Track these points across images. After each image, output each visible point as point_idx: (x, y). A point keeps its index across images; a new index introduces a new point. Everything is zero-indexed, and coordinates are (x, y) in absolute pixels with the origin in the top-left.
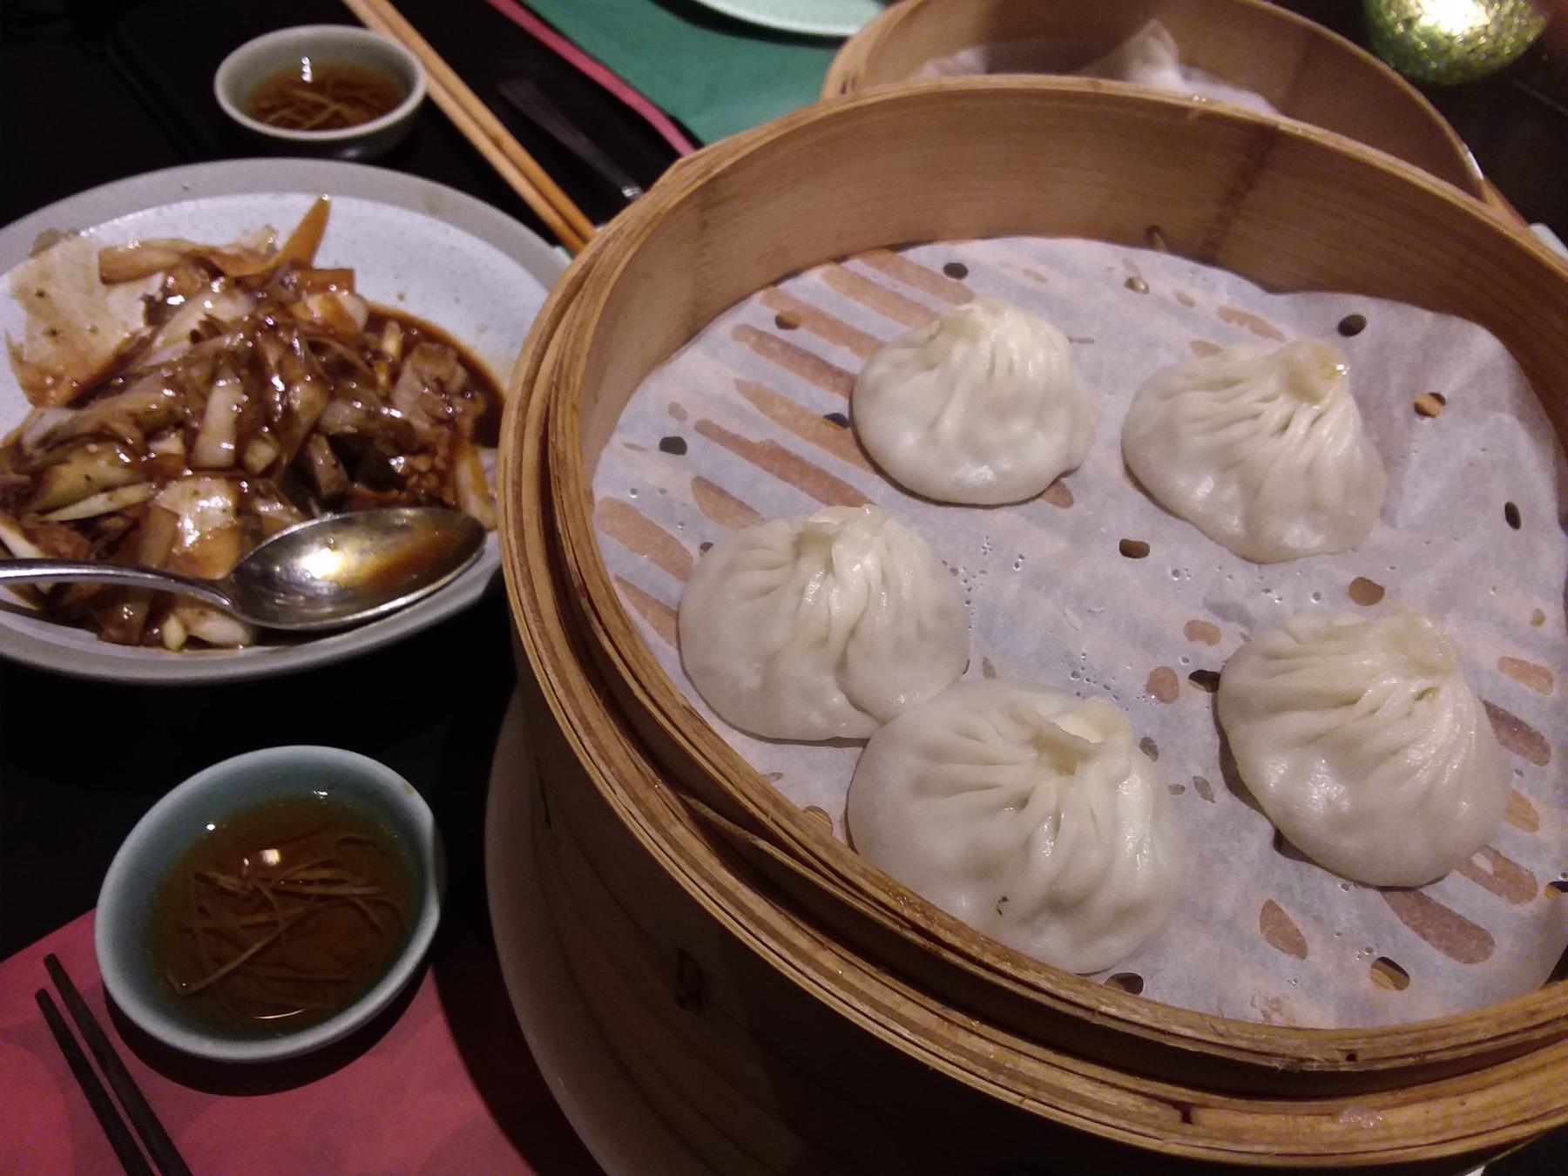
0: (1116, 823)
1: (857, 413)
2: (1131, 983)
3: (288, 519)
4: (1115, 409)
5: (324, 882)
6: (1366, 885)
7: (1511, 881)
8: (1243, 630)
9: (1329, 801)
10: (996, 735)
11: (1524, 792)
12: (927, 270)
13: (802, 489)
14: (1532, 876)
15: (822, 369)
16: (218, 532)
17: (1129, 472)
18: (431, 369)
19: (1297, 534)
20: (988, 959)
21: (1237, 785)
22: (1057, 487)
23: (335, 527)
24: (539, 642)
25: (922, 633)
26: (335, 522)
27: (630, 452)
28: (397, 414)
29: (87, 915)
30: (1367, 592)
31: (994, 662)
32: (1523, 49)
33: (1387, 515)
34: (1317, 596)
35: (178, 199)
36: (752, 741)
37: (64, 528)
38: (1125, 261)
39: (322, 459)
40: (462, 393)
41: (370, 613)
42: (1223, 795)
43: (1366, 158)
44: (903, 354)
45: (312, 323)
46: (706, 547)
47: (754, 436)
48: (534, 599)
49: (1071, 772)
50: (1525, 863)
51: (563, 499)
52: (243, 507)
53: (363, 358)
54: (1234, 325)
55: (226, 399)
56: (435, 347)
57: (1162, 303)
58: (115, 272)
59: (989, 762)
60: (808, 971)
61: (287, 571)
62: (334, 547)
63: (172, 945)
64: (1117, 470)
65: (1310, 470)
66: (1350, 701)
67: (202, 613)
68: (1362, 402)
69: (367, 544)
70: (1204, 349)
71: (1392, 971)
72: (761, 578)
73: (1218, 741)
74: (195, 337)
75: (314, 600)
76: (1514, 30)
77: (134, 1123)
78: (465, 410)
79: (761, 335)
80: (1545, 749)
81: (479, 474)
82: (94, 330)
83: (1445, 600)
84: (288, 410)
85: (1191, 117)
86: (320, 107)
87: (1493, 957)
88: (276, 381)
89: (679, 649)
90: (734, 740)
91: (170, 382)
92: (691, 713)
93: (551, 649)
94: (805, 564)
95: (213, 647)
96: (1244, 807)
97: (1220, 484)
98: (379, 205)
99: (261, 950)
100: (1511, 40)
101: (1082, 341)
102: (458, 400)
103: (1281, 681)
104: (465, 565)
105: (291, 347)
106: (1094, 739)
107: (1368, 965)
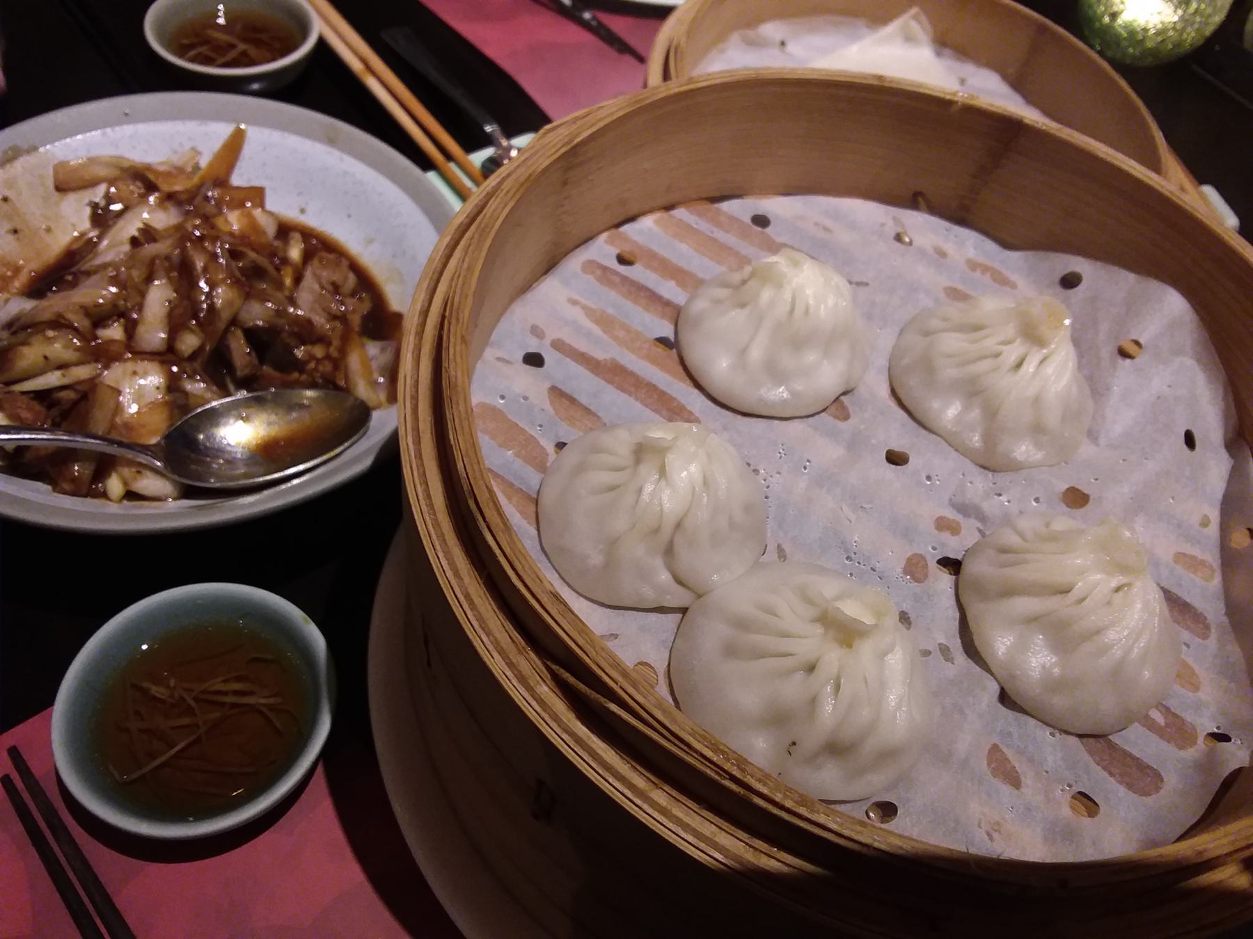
0: (883, 685)
1: (682, 337)
2: (887, 810)
3: (209, 395)
4: (885, 340)
5: (236, 693)
6: (1067, 733)
7: (1177, 731)
8: (979, 525)
9: (1044, 667)
10: (791, 614)
11: (1190, 661)
12: (737, 220)
13: (637, 399)
14: (1194, 728)
15: (653, 299)
16: (153, 405)
17: (894, 393)
18: (327, 275)
19: (1023, 450)
20: (788, 804)
21: (972, 650)
22: (839, 405)
23: (246, 403)
24: (432, 532)
25: (732, 525)
26: (246, 400)
27: (499, 364)
28: (300, 312)
29: (44, 713)
30: (1076, 498)
31: (787, 547)
32: (1201, 43)
33: (1092, 435)
34: (1037, 500)
35: (119, 123)
36: (595, 606)
37: (24, 397)
38: (894, 218)
39: (240, 349)
40: (353, 294)
41: (276, 476)
42: (960, 658)
43: (1090, 148)
44: (722, 293)
45: (231, 234)
46: (561, 446)
47: (599, 355)
48: (428, 496)
49: (850, 646)
50: (1189, 717)
51: (454, 414)
52: (173, 386)
53: (272, 263)
54: (978, 274)
55: (159, 296)
56: (332, 256)
57: (922, 252)
58: (67, 182)
59: (785, 635)
60: (645, 807)
61: (207, 437)
62: (246, 419)
63: (113, 743)
64: (884, 391)
65: (1037, 401)
66: (1065, 591)
67: (139, 472)
68: (1076, 342)
69: (273, 418)
70: (955, 295)
71: (1086, 802)
72: (606, 478)
73: (957, 615)
74: (134, 242)
75: (231, 462)
76: (1196, 26)
77: (79, 879)
78: (356, 309)
79: (605, 269)
80: (1207, 627)
81: (366, 363)
82: (48, 230)
83: (1139, 505)
84: (212, 307)
85: (954, 109)
86: (232, 46)
87: (1162, 792)
88: (202, 284)
89: (538, 530)
90: (580, 606)
91: (114, 281)
92: (556, 597)
93: (441, 536)
94: (643, 469)
95: (149, 504)
96: (978, 669)
97: (967, 408)
98: (286, 134)
99: (189, 748)
100: (1193, 34)
101: (859, 284)
102: (350, 301)
103: (1008, 571)
104: (355, 438)
105: (214, 256)
106: (868, 620)
107: (1069, 796)
